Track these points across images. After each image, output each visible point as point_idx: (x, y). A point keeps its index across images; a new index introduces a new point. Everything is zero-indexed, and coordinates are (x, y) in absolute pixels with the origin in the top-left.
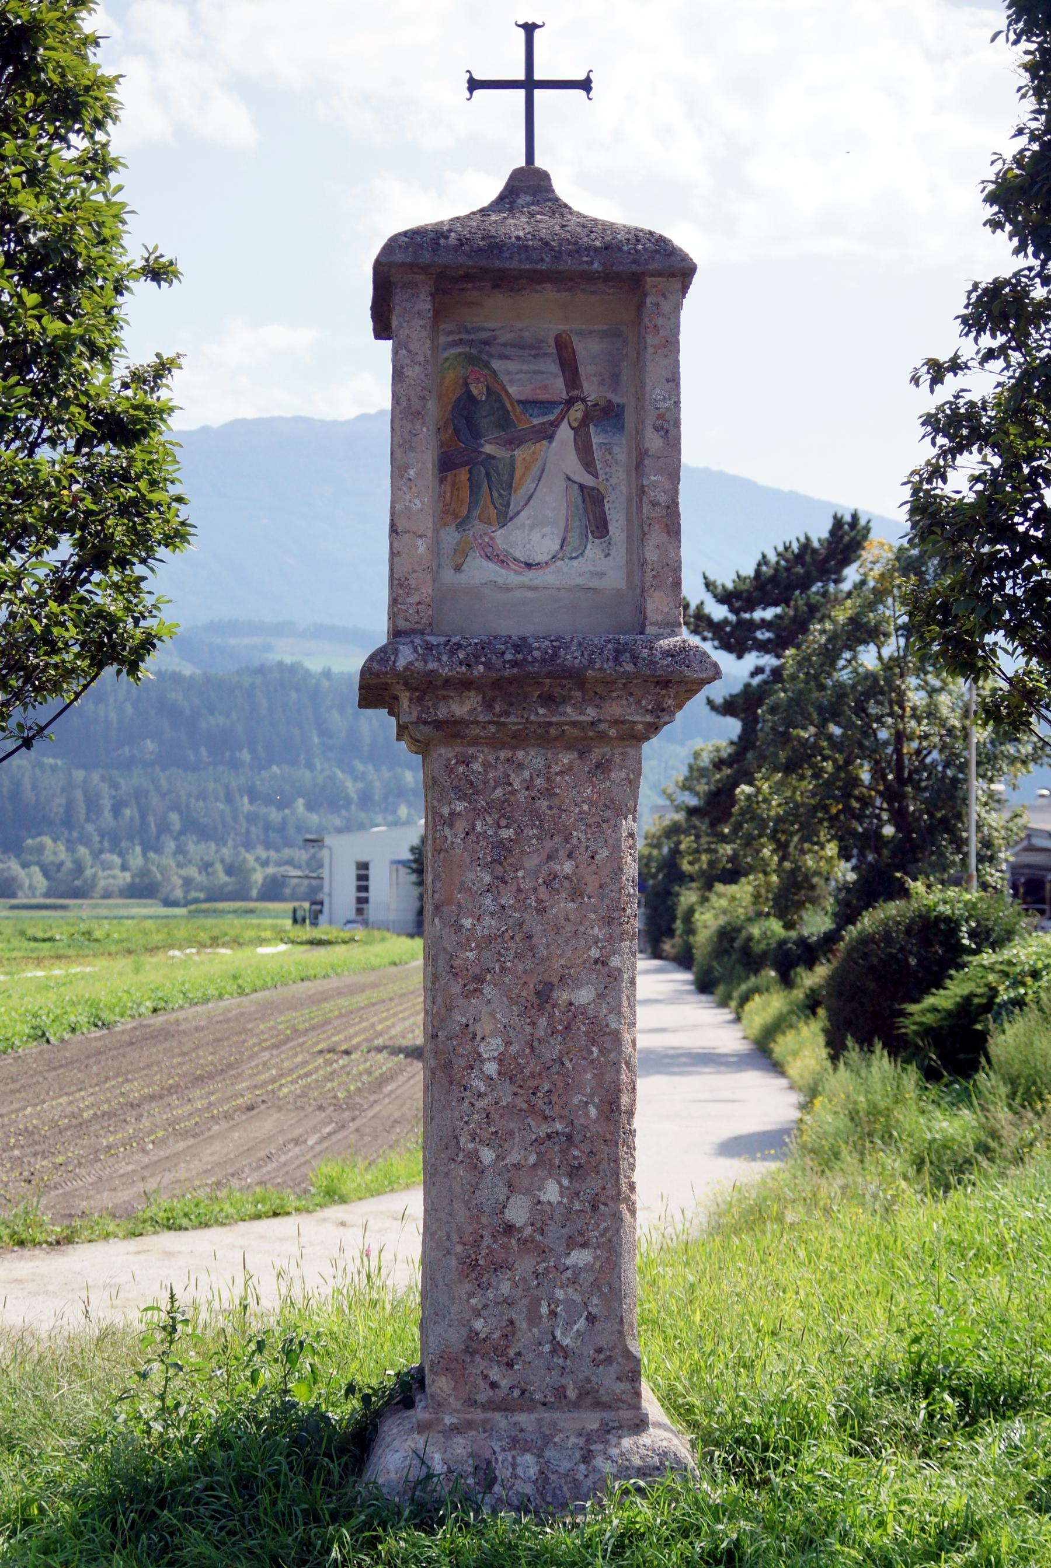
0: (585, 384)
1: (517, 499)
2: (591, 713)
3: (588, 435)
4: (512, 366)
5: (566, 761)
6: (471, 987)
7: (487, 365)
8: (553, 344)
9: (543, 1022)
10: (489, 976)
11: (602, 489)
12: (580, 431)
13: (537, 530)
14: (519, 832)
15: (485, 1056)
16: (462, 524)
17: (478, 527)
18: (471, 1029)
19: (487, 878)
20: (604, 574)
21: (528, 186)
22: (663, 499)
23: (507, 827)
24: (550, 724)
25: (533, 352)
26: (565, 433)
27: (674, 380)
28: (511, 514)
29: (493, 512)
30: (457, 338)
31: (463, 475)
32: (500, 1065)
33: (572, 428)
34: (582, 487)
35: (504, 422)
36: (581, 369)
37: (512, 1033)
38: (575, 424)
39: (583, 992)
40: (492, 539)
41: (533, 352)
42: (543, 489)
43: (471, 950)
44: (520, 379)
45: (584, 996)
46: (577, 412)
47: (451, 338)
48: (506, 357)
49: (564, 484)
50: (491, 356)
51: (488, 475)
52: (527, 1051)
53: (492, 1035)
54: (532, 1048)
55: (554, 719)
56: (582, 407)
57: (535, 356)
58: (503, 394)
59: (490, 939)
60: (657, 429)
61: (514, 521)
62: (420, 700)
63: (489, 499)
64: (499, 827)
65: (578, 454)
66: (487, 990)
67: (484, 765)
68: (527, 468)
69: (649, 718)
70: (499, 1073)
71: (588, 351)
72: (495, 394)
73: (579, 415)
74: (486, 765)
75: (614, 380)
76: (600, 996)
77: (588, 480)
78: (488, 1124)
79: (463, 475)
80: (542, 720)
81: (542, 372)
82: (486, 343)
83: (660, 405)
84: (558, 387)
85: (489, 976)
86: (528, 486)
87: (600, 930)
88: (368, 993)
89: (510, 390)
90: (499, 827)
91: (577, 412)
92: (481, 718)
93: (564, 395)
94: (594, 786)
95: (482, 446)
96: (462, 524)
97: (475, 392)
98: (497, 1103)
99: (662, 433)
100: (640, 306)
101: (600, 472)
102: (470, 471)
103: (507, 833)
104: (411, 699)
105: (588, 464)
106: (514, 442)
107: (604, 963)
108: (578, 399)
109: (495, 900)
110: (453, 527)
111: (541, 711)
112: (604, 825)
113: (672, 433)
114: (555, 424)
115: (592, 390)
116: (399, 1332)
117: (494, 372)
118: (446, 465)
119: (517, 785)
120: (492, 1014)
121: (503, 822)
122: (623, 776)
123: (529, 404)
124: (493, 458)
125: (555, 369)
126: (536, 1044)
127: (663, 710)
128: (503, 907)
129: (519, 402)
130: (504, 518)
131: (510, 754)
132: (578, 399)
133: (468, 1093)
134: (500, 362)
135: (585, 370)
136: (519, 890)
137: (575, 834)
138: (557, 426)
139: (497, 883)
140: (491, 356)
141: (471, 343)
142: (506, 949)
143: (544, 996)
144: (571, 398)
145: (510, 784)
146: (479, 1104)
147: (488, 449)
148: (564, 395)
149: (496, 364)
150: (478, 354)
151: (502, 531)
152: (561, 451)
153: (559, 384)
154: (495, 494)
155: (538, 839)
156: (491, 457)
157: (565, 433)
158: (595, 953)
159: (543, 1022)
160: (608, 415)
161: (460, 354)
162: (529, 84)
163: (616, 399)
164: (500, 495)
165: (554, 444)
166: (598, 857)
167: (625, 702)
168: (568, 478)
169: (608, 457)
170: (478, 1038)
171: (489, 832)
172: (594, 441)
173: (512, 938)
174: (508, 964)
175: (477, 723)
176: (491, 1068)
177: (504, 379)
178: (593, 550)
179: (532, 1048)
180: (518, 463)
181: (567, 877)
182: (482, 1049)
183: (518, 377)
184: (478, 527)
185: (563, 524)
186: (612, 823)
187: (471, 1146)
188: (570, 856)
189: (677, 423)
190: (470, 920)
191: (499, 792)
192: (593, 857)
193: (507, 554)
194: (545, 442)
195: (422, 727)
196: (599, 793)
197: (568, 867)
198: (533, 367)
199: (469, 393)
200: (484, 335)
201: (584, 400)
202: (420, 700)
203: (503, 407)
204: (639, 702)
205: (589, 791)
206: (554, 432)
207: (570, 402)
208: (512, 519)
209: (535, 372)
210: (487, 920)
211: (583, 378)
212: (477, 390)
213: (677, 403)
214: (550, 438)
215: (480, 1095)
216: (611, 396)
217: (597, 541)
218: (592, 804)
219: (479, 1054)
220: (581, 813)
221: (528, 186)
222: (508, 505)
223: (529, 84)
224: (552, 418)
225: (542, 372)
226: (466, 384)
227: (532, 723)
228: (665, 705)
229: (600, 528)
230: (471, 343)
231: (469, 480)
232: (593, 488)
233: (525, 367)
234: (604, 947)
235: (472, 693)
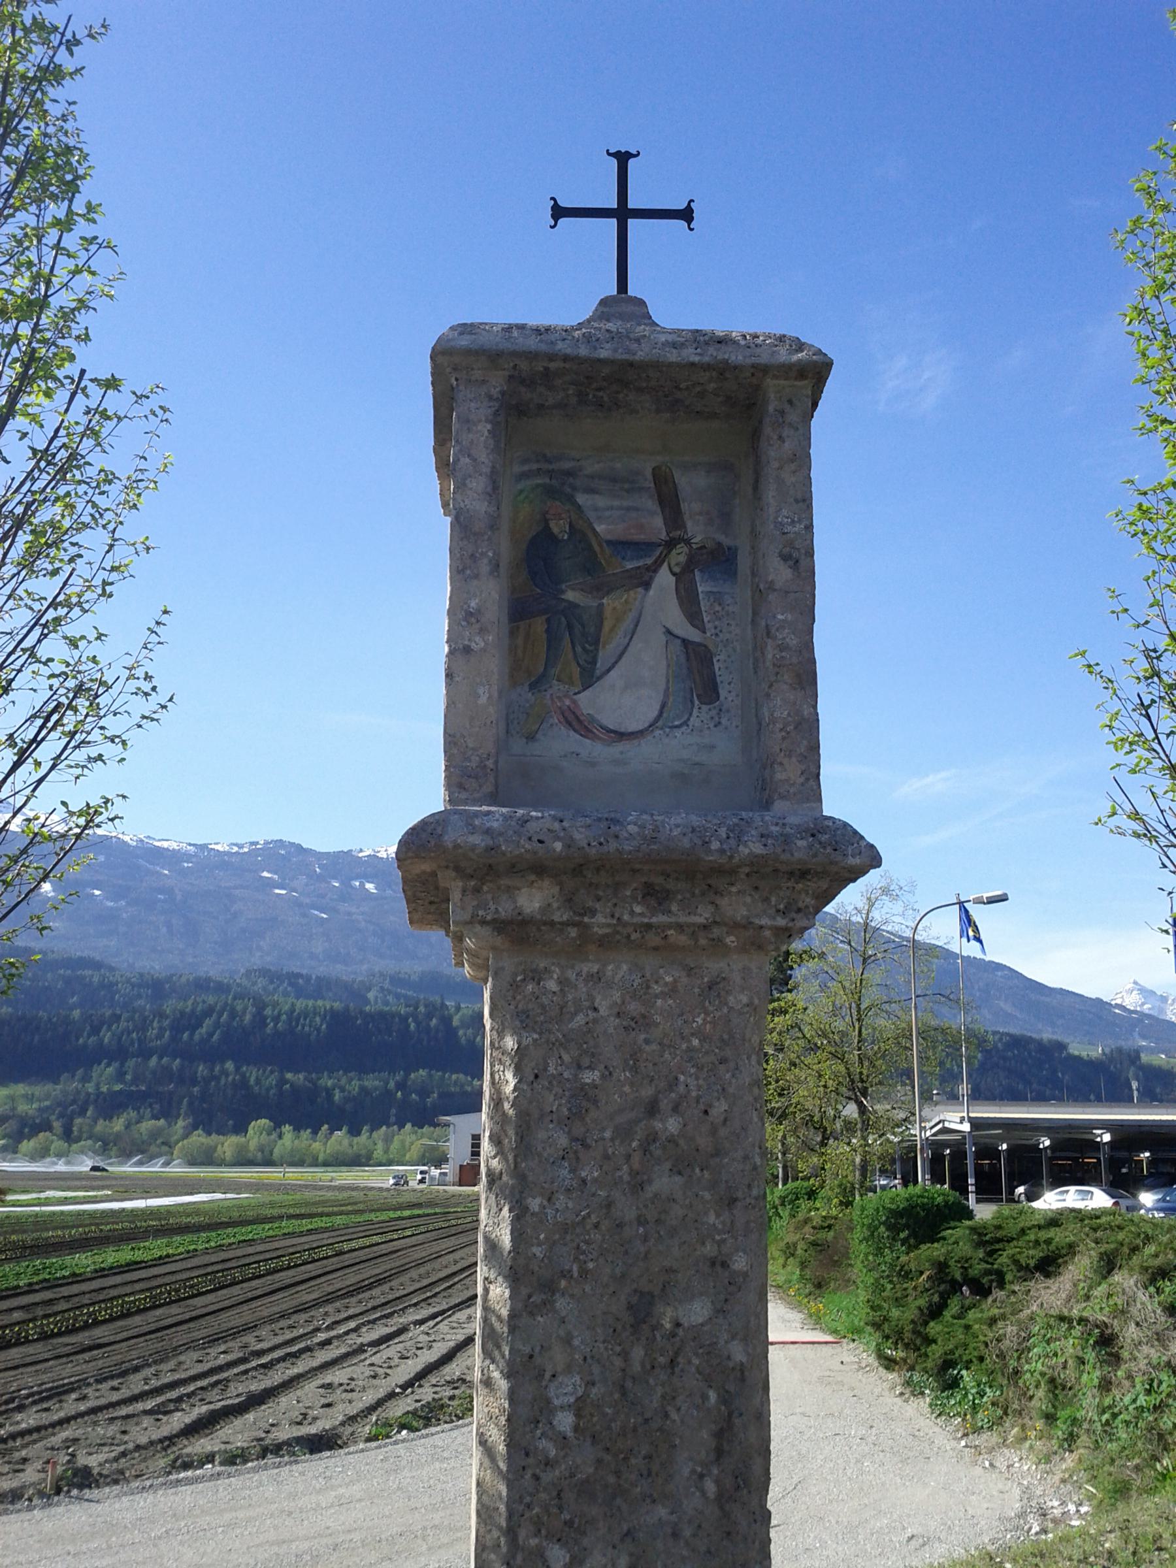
0: (689, 524)
1: (605, 656)
2: (703, 915)
3: (693, 582)
4: (601, 501)
5: (668, 979)
6: (537, 1299)
7: (571, 499)
8: (650, 477)
9: (638, 1353)
10: (563, 1283)
11: (711, 647)
12: (684, 578)
13: (631, 689)
14: (608, 1074)
15: (556, 1402)
16: (536, 685)
17: (557, 688)
18: (538, 1360)
19: (563, 1141)
20: (713, 747)
21: (622, 304)
22: (793, 641)
23: (591, 1068)
24: (649, 927)
25: (626, 486)
26: (664, 579)
27: (805, 502)
28: (598, 673)
29: (576, 671)
30: (535, 466)
31: (539, 625)
32: (578, 1415)
33: (674, 574)
34: (685, 642)
35: (591, 566)
36: (684, 506)
37: (596, 1369)
38: (677, 570)
39: (697, 1306)
40: (574, 702)
41: (626, 486)
42: (636, 645)
43: (539, 1245)
44: (608, 517)
45: (697, 1312)
46: (679, 556)
47: (526, 468)
48: (591, 491)
49: (663, 638)
50: (574, 489)
51: (570, 627)
52: (617, 1396)
53: (569, 1369)
54: (624, 1392)
55: (654, 920)
56: (686, 549)
57: (628, 491)
58: (590, 535)
59: (565, 1229)
60: (785, 558)
61: (601, 682)
62: (477, 890)
63: (571, 655)
64: (579, 1067)
65: (681, 604)
66: (561, 1303)
67: (560, 982)
68: (618, 620)
69: (781, 922)
70: (576, 1429)
71: (692, 485)
72: (580, 535)
73: (682, 559)
74: (563, 982)
75: (725, 518)
76: (720, 1312)
77: (694, 635)
78: (560, 1508)
79: (539, 625)
80: (636, 920)
81: (637, 509)
82: (569, 473)
83: (789, 529)
84: (656, 526)
85: (563, 1283)
86: (618, 640)
87: (718, 1216)
88: (105, 1292)
89: (598, 529)
90: (579, 1067)
91: (679, 556)
92: (557, 917)
93: (663, 536)
94: (707, 1013)
95: (563, 592)
96: (536, 685)
97: (556, 530)
98: (572, 1475)
99: (791, 563)
100: (755, 435)
101: (708, 626)
102: (548, 621)
103: (589, 1077)
104: (464, 891)
105: (694, 617)
106: (602, 589)
107: (724, 1265)
108: (680, 540)
109: (573, 1171)
110: (526, 688)
111: (638, 909)
112: (722, 1067)
113: (803, 562)
114: (654, 568)
115: (697, 531)
116: (588, 821)
117: (580, 507)
118: (519, 611)
119: (603, 1011)
120: (567, 1341)
121: (586, 1061)
122: (745, 1000)
123: (622, 546)
124: (577, 606)
125: (651, 504)
126: (629, 1384)
127: (799, 910)
128: (584, 1181)
129: (609, 542)
130: (589, 677)
131: (595, 968)
132: (680, 540)
133: (531, 1460)
134: (586, 496)
135: (690, 507)
136: (606, 1157)
137: (682, 1078)
138: (655, 571)
139: (577, 1146)
140: (574, 489)
141: (550, 473)
142: (587, 1243)
143: (641, 1312)
144: (672, 539)
145: (595, 1009)
146: (548, 1477)
147: (570, 596)
148: (663, 536)
149: (581, 499)
150: (558, 486)
151: (587, 693)
152: (661, 599)
153: (658, 522)
154: (579, 649)
155: (632, 1084)
156: (573, 606)
157: (664, 579)
158: (709, 1249)
159: (638, 1353)
160: (720, 560)
161: (538, 486)
162: (623, 213)
163: (726, 541)
164: (584, 648)
165: (651, 593)
166: (714, 1112)
167: (748, 899)
168: (669, 632)
169: (718, 608)
170: (547, 1375)
171: (566, 1075)
172: (700, 590)
173: (596, 1226)
174: (591, 1265)
175: (552, 924)
176: (565, 1421)
177: (591, 515)
178: (701, 715)
179: (624, 1392)
180: (608, 613)
181: (672, 1140)
182: (552, 1393)
183: (607, 513)
184: (557, 688)
185: (662, 687)
186: (732, 1065)
187: (534, 1542)
188: (676, 1109)
189: (810, 553)
190: (538, 1201)
191: (580, 1019)
192: (706, 1112)
193: (592, 719)
194: (640, 590)
195: (478, 928)
196: (714, 1023)
197: (672, 1125)
198: (625, 504)
199: (547, 528)
200: (567, 465)
201: (688, 542)
202: (477, 890)
203: (590, 548)
204: (766, 900)
205: (699, 1020)
206: (651, 579)
207: (671, 544)
208: (599, 679)
209: (628, 509)
210: (561, 1200)
211: (686, 517)
212: (559, 528)
213: (810, 527)
214: (647, 585)
215: (548, 1463)
216: (721, 538)
217: (705, 708)
218: (704, 1039)
219: (548, 1401)
220: (690, 1049)
221: (622, 304)
222: (594, 662)
223: (623, 213)
224: (649, 561)
225: (637, 509)
226: (546, 521)
227: (625, 925)
228: (801, 905)
229: (709, 691)
230: (550, 473)
231: (547, 631)
232: (699, 644)
233: (616, 503)
234: (724, 1241)
235: (546, 883)
